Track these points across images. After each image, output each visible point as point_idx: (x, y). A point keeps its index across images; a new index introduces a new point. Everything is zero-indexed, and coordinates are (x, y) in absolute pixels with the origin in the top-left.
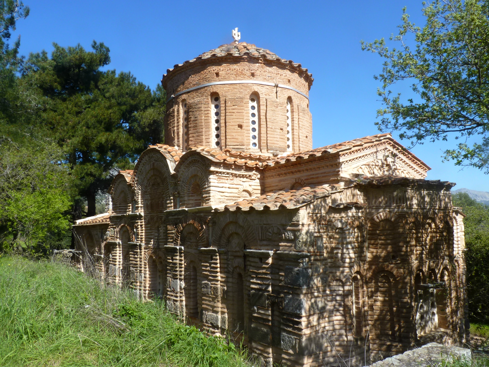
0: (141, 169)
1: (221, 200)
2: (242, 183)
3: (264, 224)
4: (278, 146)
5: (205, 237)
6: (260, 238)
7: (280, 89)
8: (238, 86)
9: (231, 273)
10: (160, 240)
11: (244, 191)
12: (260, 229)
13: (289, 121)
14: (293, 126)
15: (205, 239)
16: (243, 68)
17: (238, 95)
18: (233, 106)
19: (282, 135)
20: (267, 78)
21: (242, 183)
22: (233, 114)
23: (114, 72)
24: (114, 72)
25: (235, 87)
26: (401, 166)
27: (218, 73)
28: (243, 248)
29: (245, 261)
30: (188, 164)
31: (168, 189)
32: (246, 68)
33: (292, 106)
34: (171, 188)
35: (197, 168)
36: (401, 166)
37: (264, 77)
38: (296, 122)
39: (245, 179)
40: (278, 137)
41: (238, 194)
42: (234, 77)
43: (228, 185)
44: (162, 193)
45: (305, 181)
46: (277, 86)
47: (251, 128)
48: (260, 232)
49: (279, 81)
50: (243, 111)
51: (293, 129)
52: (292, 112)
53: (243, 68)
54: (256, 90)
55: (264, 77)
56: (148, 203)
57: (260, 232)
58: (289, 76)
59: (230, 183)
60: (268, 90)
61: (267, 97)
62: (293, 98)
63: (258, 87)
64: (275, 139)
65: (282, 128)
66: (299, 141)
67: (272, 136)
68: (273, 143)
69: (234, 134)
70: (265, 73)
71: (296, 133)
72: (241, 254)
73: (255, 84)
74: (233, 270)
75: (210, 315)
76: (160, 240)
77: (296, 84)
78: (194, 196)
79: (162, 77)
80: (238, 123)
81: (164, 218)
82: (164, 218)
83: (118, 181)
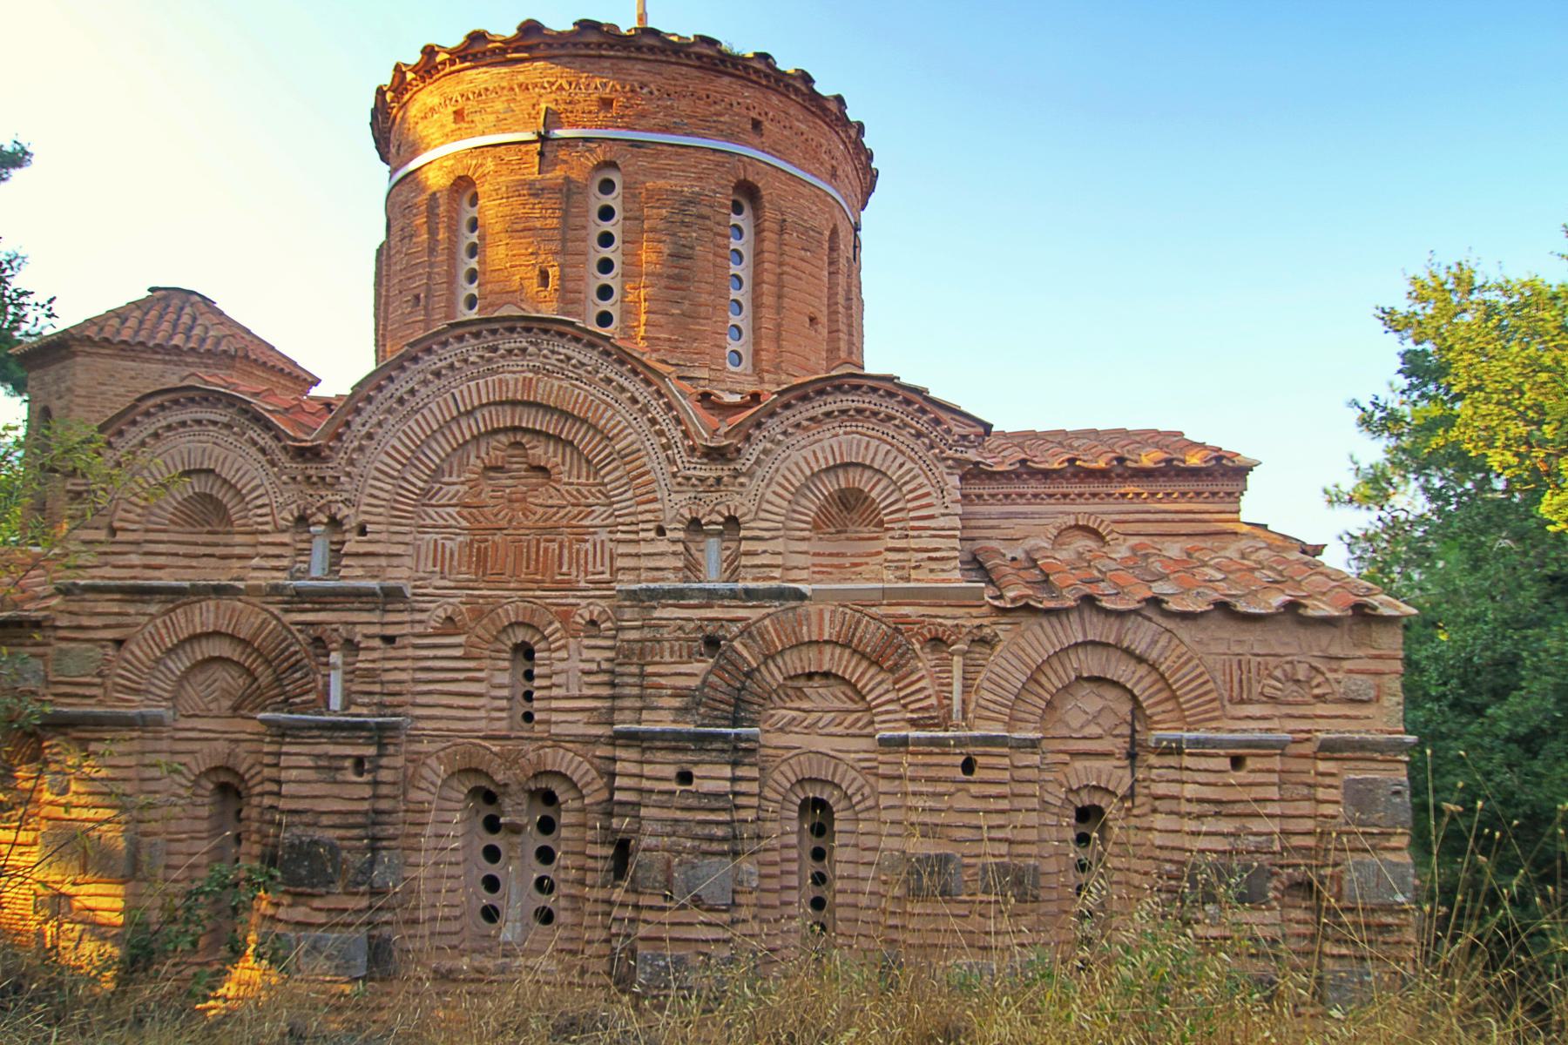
8: (806, 191)
12: (1235, 667)
18: (803, 249)
45: (1113, 526)
48: (1236, 680)
57: (1236, 680)
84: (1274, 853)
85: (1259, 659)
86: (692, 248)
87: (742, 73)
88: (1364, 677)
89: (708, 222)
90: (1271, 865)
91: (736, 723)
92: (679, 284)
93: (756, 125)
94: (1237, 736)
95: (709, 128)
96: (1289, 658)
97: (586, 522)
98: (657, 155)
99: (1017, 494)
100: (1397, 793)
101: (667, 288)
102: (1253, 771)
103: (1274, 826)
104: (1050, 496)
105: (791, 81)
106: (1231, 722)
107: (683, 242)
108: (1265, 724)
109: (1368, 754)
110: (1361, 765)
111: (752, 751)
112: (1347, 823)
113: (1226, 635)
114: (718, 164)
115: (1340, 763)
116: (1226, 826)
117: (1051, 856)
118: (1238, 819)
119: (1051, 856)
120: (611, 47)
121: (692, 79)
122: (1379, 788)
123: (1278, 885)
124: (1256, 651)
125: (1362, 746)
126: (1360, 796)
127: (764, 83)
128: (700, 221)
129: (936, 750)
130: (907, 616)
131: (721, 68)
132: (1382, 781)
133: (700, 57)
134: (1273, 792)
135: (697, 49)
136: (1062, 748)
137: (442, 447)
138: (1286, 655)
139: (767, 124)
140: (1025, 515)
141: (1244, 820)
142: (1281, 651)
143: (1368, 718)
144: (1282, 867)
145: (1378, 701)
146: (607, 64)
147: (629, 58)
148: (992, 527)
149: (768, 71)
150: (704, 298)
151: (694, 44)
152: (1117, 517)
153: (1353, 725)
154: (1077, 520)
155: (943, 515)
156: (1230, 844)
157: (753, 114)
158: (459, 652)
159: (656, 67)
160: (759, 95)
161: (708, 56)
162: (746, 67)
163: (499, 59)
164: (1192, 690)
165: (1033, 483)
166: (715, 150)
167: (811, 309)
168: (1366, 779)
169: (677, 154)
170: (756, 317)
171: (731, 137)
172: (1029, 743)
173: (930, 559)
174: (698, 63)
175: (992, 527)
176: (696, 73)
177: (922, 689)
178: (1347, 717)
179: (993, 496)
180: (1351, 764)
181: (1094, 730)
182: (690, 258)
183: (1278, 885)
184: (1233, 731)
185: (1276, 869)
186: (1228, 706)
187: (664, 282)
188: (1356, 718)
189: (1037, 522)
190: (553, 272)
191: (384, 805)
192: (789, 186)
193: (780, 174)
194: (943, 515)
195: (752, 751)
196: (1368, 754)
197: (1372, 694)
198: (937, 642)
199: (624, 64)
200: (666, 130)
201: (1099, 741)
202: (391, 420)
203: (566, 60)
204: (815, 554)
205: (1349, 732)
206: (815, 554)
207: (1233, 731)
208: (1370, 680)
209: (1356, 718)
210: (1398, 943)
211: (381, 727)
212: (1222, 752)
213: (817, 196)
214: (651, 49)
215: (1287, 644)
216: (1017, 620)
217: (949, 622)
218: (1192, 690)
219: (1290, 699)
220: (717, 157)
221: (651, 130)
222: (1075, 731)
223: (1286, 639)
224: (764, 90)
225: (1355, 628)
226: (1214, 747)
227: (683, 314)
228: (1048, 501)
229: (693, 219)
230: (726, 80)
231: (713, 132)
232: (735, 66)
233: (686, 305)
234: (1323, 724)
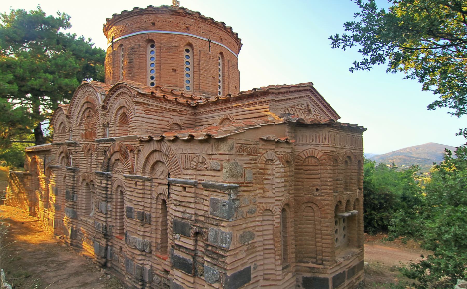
0: (77, 103)
1: (148, 130)
2: (172, 117)
3: (189, 154)
4: (210, 91)
5: (130, 164)
6: (184, 166)
7: (213, 44)
8: (173, 36)
9: (155, 199)
10: (93, 166)
11: (174, 124)
12: (184, 157)
13: (220, 73)
14: (223, 76)
15: (131, 167)
16: (178, 21)
17: (173, 44)
18: (168, 52)
19: (214, 82)
20: (202, 33)
21: (172, 117)
22: (167, 59)
23: (75, 35)
24: (75, 35)
25: (170, 36)
26: (319, 113)
27: (154, 23)
28: (168, 176)
29: (169, 189)
30: (116, 96)
31: (99, 120)
32: (182, 22)
33: (223, 61)
34: (102, 119)
35: (125, 100)
36: (319, 113)
37: (198, 32)
38: (226, 74)
39: (175, 114)
40: (210, 83)
41: (168, 126)
42: (169, 28)
43: (156, 117)
44: (95, 124)
45: (234, 117)
46: (210, 41)
47: (185, 73)
48: (184, 162)
49: (212, 38)
50: (178, 58)
51: (223, 79)
52: (223, 65)
53: (178, 21)
54: (190, 42)
55: (198, 32)
56: (83, 133)
57: (184, 162)
58: (221, 36)
59: (159, 115)
60: (202, 44)
61: (201, 49)
62: (224, 54)
63: (193, 40)
64: (208, 85)
65: (214, 76)
66: (229, 89)
67: (204, 81)
68: (205, 88)
69: (168, 77)
70: (199, 29)
71: (226, 82)
72: (165, 182)
73: (191, 36)
74: (158, 197)
75: (134, 238)
76: (93, 166)
77: (228, 44)
78: (123, 126)
79: (103, 26)
80: (173, 67)
81: (95, 146)
82: (95, 146)
83: (59, 114)
84: (192, 220)
85: (190, 155)
86: (133, 59)
87: (148, 12)
88: (217, 161)
89: (136, 52)
90: (191, 225)
91: (108, 171)
92: (131, 69)
93: (153, 24)
94: (184, 180)
95: (140, 29)
96: (197, 155)
97: (96, 126)
98: (129, 40)
99: (211, 110)
100: (224, 205)
101: (129, 70)
102: (187, 192)
103: (193, 211)
104: (219, 110)
105: (162, 9)
106: (183, 175)
107: (131, 59)
108: (191, 177)
109: (216, 190)
110: (215, 193)
111: (110, 178)
112: (211, 214)
113: (182, 147)
114: (142, 37)
115: (209, 192)
116: (181, 209)
117: (154, 212)
118: (185, 207)
119: (154, 212)
120: (121, 18)
121: (137, 18)
122: (219, 203)
123: (193, 232)
124: (189, 152)
125: (213, 186)
126: (214, 204)
127: (154, 12)
128: (134, 53)
129: (131, 179)
130: (128, 144)
131: (142, 13)
132: (220, 200)
133: (136, 12)
134: (192, 200)
135: (135, 11)
136: (157, 181)
137: (81, 113)
138: (196, 154)
139: (156, 23)
140: (213, 117)
141: (186, 208)
142: (195, 152)
143: (218, 176)
144: (194, 226)
145: (222, 171)
146: (121, 22)
147: (124, 19)
148: (206, 121)
149: (153, 9)
150: (136, 71)
151: (161, 8)
152: (234, 114)
153: (212, 179)
154: (225, 116)
155: (135, 117)
156: (182, 215)
157: (151, 22)
158: (83, 155)
159: (129, 19)
160: (154, 16)
161: (138, 12)
162: (148, 11)
163: (109, 29)
164: (175, 165)
165: (214, 106)
166: (141, 34)
167: (173, 67)
168: (216, 199)
169: (134, 38)
170: (223, 72)
171: (145, 29)
172: (146, 179)
173: (132, 129)
174: (137, 14)
175: (206, 121)
176: (137, 17)
177: (129, 163)
178: (212, 176)
179: (206, 112)
180: (212, 193)
181: (162, 177)
182: (132, 62)
183: (193, 232)
184: (183, 179)
185: (192, 226)
186: (183, 170)
187: (128, 69)
188: (214, 176)
189: (216, 118)
190: (112, 72)
191: (75, 185)
192: (165, 36)
193: (161, 35)
194: (135, 117)
195: (110, 178)
196: (216, 190)
197: (220, 168)
198: (131, 151)
199: (124, 21)
200: (131, 33)
201: (163, 180)
202: (76, 108)
203: (117, 24)
204: (124, 130)
205: (211, 181)
206: (124, 130)
207: (183, 179)
208: (219, 163)
209: (214, 176)
210: (223, 262)
211: (74, 170)
212: (179, 185)
213: (178, 37)
214: (127, 15)
215: (197, 150)
216: (144, 144)
217: (133, 146)
218: (175, 165)
219: (200, 169)
220: (142, 36)
221: (128, 34)
222: (158, 177)
223: (196, 148)
224: (155, 14)
225: (216, 143)
226: (178, 183)
227: (132, 76)
228: (218, 111)
229: (133, 53)
230: (144, 16)
231: (141, 29)
232: (145, 11)
233: (132, 74)
234: (205, 178)
